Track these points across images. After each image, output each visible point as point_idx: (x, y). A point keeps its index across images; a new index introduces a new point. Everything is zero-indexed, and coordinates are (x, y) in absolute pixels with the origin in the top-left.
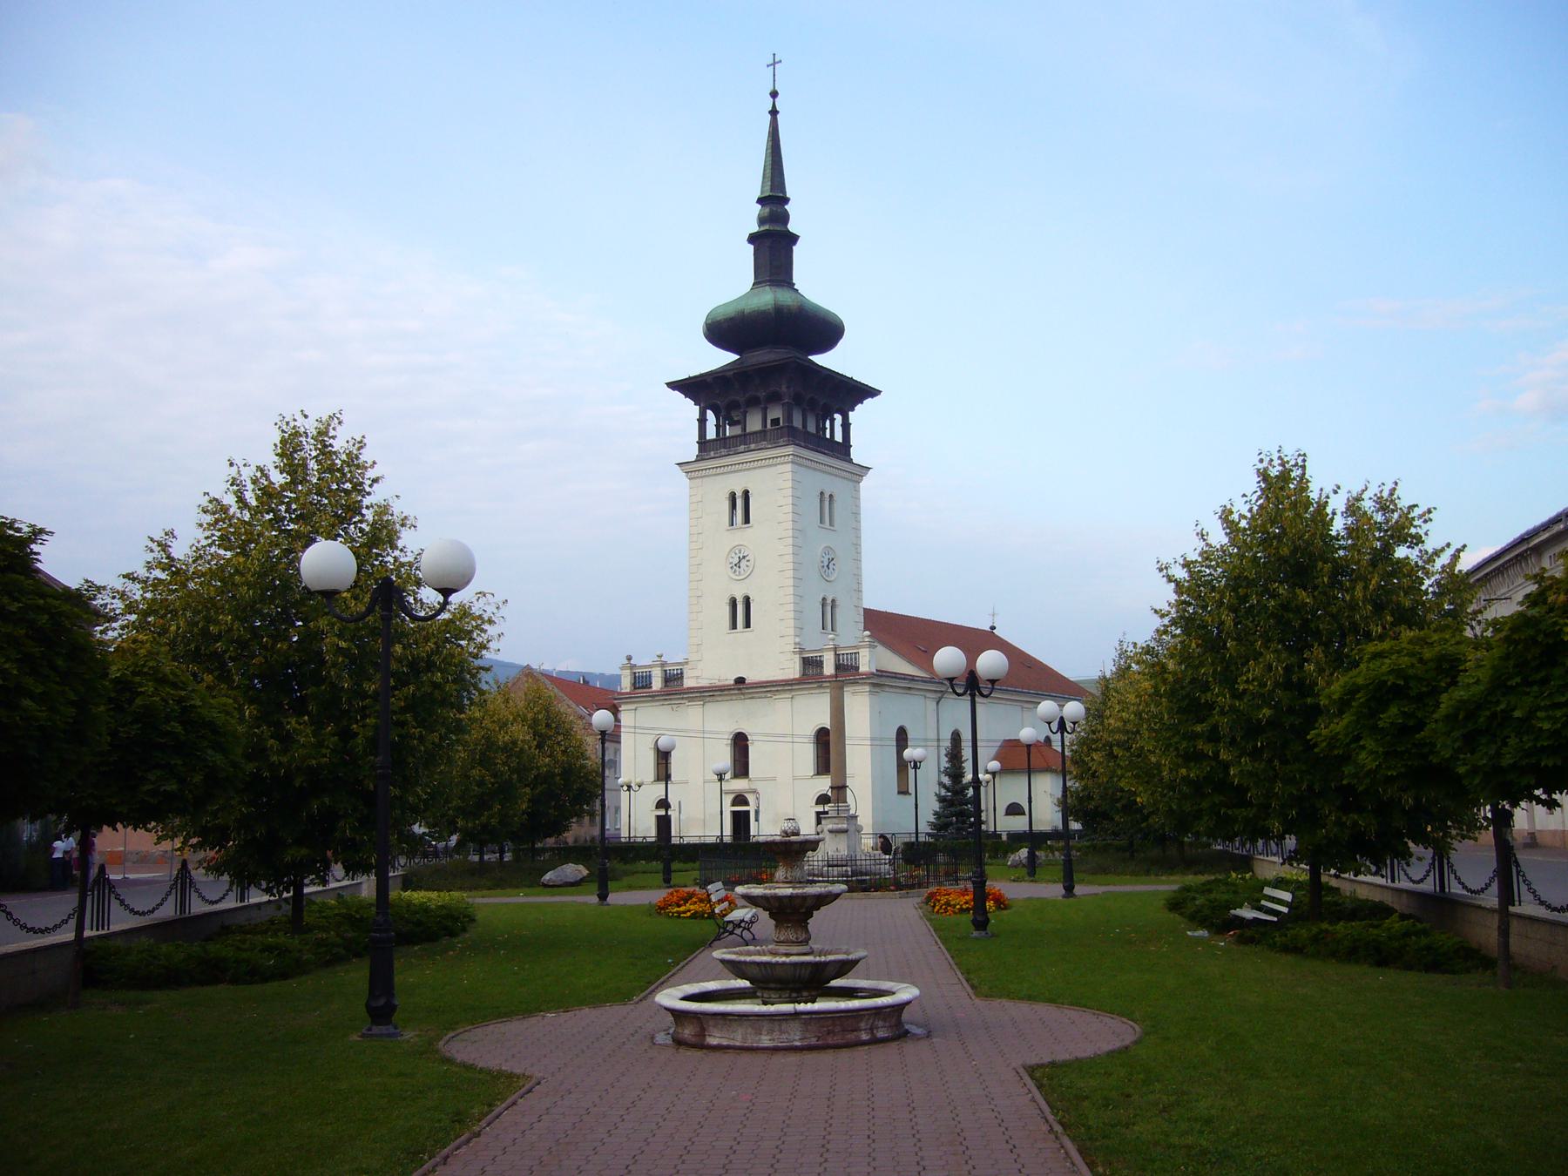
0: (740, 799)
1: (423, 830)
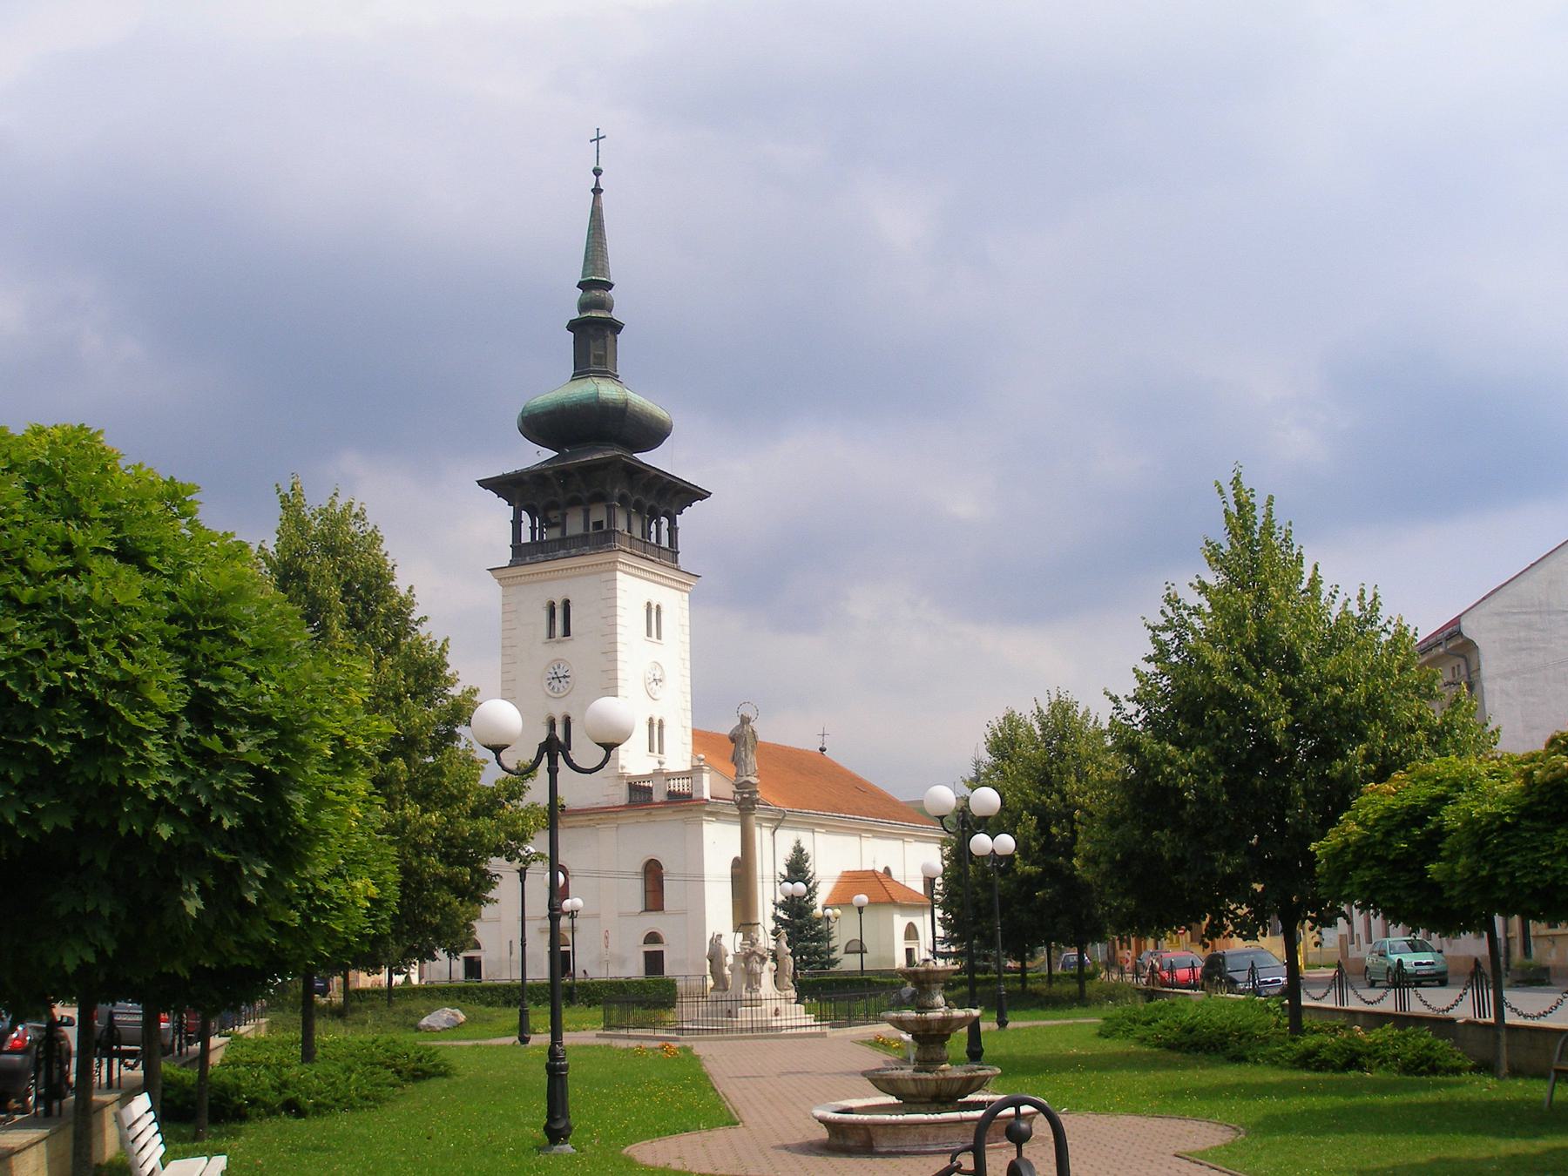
0: (653, 938)
1: (1255, 886)
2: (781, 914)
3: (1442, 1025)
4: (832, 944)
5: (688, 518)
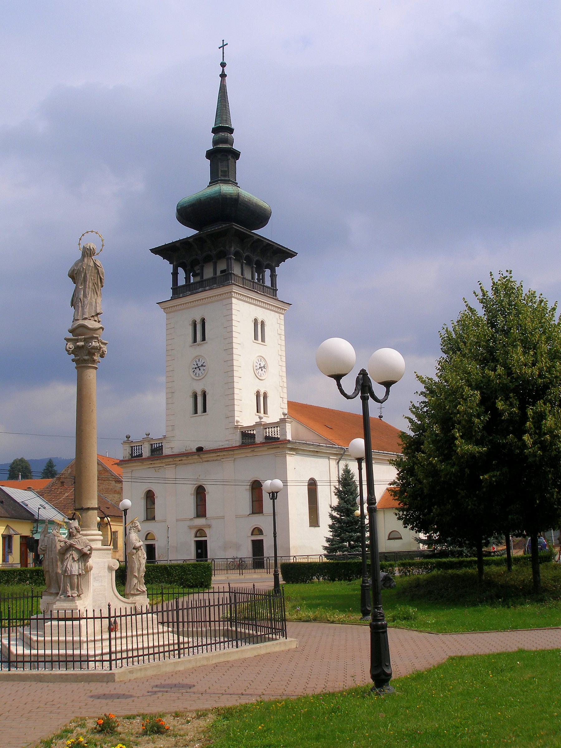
2: (335, 514)
5: (282, 269)
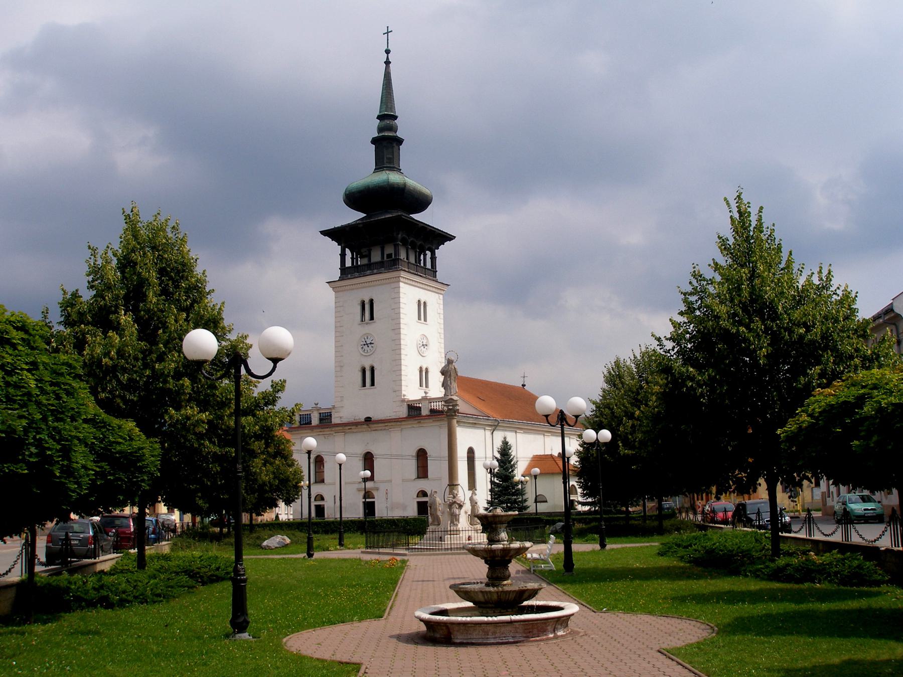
3: (870, 552)
4: (525, 497)
5: (443, 251)
